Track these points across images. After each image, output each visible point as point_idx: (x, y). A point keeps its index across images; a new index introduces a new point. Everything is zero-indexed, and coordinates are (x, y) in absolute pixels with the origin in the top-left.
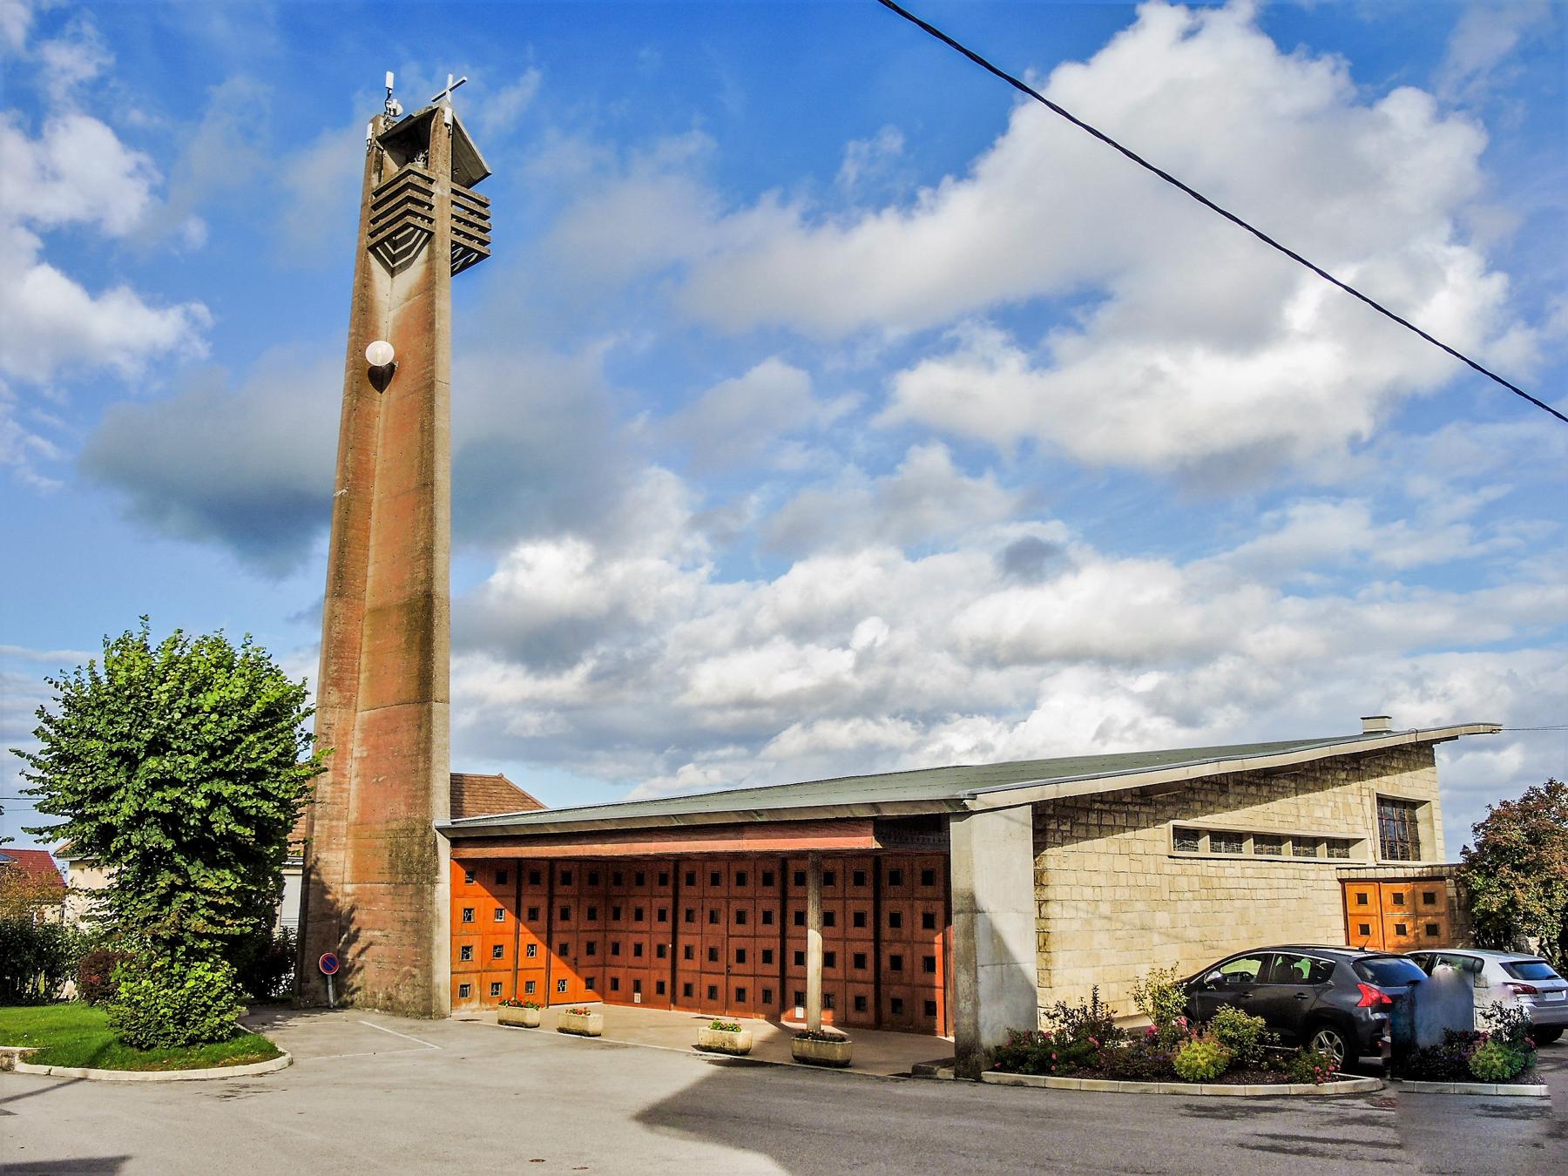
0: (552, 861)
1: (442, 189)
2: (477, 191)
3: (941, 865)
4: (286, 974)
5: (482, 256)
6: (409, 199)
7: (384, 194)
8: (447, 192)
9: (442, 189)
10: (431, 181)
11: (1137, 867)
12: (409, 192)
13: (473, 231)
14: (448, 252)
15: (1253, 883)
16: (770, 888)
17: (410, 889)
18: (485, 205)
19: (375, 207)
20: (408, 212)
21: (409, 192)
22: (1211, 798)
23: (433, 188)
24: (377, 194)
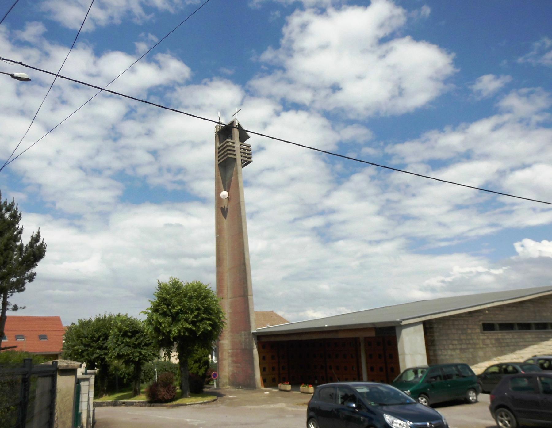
0: (327, 382)
1: (237, 145)
2: (247, 142)
3: (99, 382)
4: (198, 382)
5: (249, 162)
6: (228, 150)
7: (221, 148)
8: (239, 146)
9: (237, 145)
10: (234, 143)
11: (469, 337)
12: (228, 148)
13: (246, 151)
14: (241, 163)
15: (518, 340)
16: (81, 374)
17: (81, 348)
18: (249, 147)
19: (219, 157)
20: (228, 154)
21: (228, 148)
22: (497, 312)
23: (235, 145)
24: (219, 149)
